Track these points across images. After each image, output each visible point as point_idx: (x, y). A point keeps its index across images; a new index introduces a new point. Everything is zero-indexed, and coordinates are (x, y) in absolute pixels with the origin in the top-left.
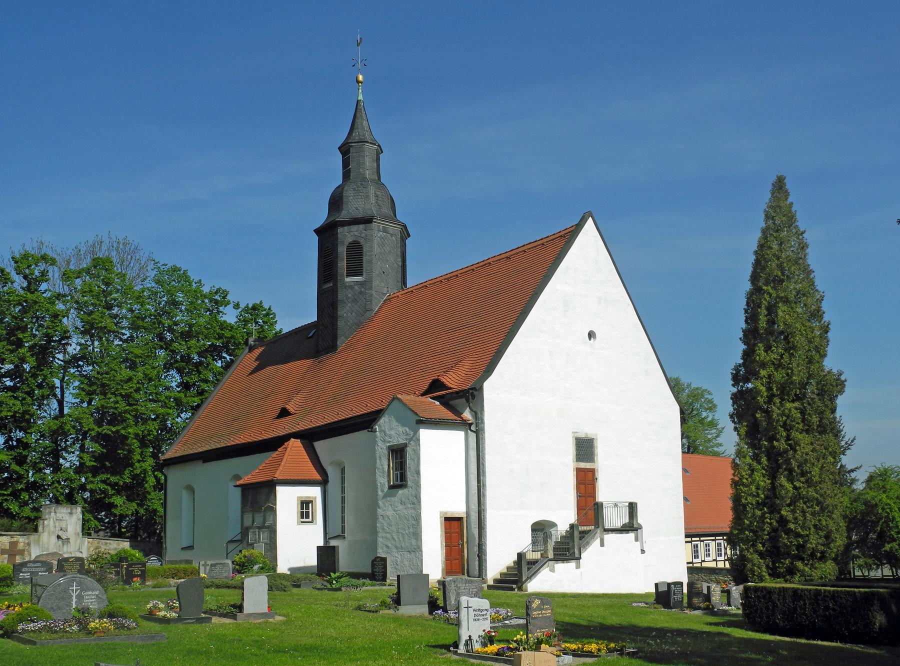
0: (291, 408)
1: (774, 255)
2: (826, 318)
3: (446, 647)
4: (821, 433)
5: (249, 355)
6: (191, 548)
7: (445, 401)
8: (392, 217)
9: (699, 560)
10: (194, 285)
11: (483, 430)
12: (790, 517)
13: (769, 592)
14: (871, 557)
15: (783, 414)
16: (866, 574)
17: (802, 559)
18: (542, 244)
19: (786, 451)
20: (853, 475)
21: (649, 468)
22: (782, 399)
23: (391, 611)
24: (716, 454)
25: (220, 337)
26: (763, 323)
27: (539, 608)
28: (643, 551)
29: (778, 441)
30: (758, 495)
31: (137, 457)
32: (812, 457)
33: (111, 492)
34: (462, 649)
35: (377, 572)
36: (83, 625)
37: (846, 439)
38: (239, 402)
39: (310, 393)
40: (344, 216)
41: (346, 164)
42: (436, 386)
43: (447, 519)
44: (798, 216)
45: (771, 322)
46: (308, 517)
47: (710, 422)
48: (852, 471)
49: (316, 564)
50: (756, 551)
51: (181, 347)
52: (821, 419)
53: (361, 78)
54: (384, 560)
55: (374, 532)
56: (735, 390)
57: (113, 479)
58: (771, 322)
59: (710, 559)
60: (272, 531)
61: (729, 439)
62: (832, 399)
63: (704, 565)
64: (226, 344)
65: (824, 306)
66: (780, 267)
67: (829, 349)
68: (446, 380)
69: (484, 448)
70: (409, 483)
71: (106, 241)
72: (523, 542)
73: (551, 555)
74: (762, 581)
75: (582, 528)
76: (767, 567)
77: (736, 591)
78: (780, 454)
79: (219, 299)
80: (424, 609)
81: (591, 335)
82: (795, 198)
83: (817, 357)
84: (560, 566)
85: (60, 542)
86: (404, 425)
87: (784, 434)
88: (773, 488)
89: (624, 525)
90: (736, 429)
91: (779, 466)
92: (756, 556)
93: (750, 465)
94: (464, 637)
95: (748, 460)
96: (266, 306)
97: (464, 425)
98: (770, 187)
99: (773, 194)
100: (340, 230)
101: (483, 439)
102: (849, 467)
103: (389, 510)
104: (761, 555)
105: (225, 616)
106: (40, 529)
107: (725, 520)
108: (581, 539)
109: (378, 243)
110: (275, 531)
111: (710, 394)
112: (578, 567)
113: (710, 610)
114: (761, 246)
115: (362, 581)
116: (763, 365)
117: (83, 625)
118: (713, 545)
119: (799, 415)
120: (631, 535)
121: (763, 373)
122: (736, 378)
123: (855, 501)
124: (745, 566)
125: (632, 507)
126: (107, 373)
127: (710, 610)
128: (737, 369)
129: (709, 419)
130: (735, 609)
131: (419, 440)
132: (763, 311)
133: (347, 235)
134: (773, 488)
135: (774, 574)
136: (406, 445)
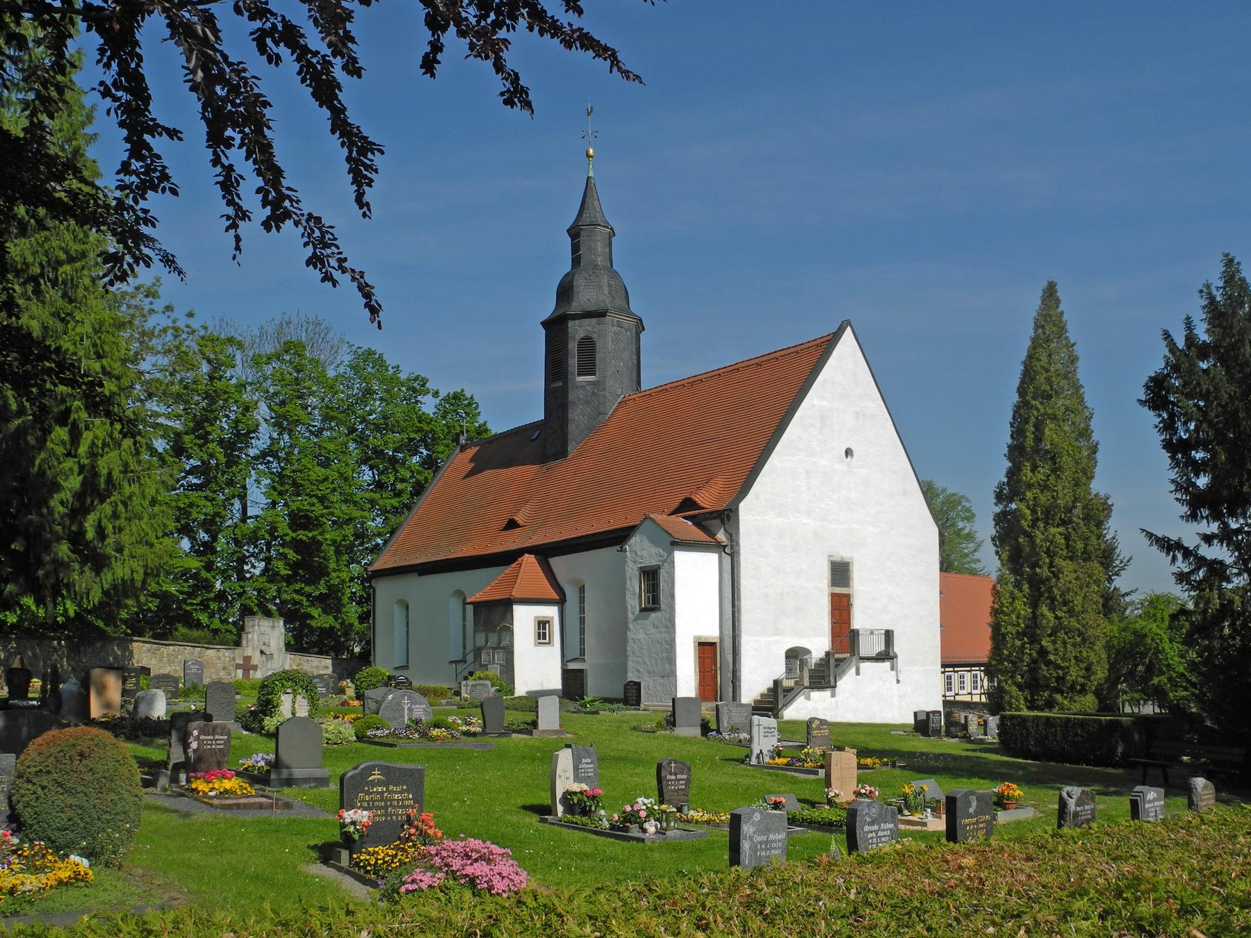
0: (519, 519)
1: (1043, 367)
2: (1095, 437)
3: (742, 762)
4: (1085, 560)
5: (461, 456)
6: (406, 667)
7: (698, 522)
8: (626, 311)
9: (952, 693)
10: (391, 371)
11: (738, 553)
12: (1050, 647)
13: (1024, 719)
14: (1138, 691)
15: (1046, 540)
16: (1136, 710)
17: (1062, 692)
18: (797, 352)
19: (1048, 579)
20: (1128, 599)
21: (905, 591)
22: (1047, 524)
23: (668, 732)
24: (973, 572)
25: (420, 430)
26: (1030, 442)
27: (818, 728)
28: (898, 681)
29: (1040, 567)
30: (1018, 625)
31: (332, 565)
32: (1075, 585)
33: (305, 603)
34: (754, 761)
35: (631, 695)
36: (424, 735)
37: (1121, 557)
38: (456, 508)
39: (540, 502)
40: (575, 308)
41: (575, 248)
42: (687, 505)
43: (701, 644)
44: (1069, 327)
45: (1038, 439)
46: (544, 638)
47: (969, 534)
48: (1127, 594)
49: (560, 687)
50: (1015, 683)
51: (374, 440)
52: (1086, 545)
53: (591, 152)
54: (638, 684)
55: (624, 656)
56: (998, 509)
57: (307, 589)
58: (1038, 439)
59: (965, 692)
60: (509, 652)
61: (989, 561)
62: (1099, 524)
63: (958, 698)
64: (429, 440)
65: (1093, 424)
66: (1048, 380)
67: (1097, 471)
68: (698, 499)
69: (739, 571)
70: (663, 606)
71: (295, 319)
72: (778, 669)
73: (806, 682)
74: (1018, 709)
75: (837, 656)
76: (1026, 699)
77: (993, 721)
78: (1043, 582)
79: (418, 387)
80: (697, 731)
81: (848, 452)
82: (1067, 307)
83: (1084, 479)
84: (815, 694)
85: (264, 658)
86: (657, 546)
87: (1047, 561)
88: (1034, 617)
89: (879, 654)
90: (997, 553)
91: (1041, 595)
92: (1014, 688)
93: (1012, 593)
94: (756, 751)
95: (1010, 587)
96: (378, 352)
97: (718, 547)
98: (1041, 294)
99: (1043, 301)
100: (571, 323)
101: (739, 561)
102: (1123, 591)
103: (640, 632)
104: (1020, 687)
105: (519, 732)
106: (244, 643)
107: (983, 650)
108: (836, 666)
109: (609, 336)
110: (512, 653)
111: (968, 501)
112: (833, 695)
113: (967, 738)
114: (1030, 357)
115: (616, 706)
116: (1030, 486)
117: (424, 735)
118: (968, 676)
119: (1063, 541)
120: (887, 664)
121: (1029, 495)
122: (1000, 497)
123: (1124, 630)
124: (1002, 698)
125: (889, 635)
126: (300, 471)
127: (967, 738)
128: (1001, 486)
129: (967, 531)
130: (992, 738)
131: (673, 562)
132: (1031, 428)
133: (578, 330)
134: (1034, 617)
135: (1030, 708)
136: (659, 567)
